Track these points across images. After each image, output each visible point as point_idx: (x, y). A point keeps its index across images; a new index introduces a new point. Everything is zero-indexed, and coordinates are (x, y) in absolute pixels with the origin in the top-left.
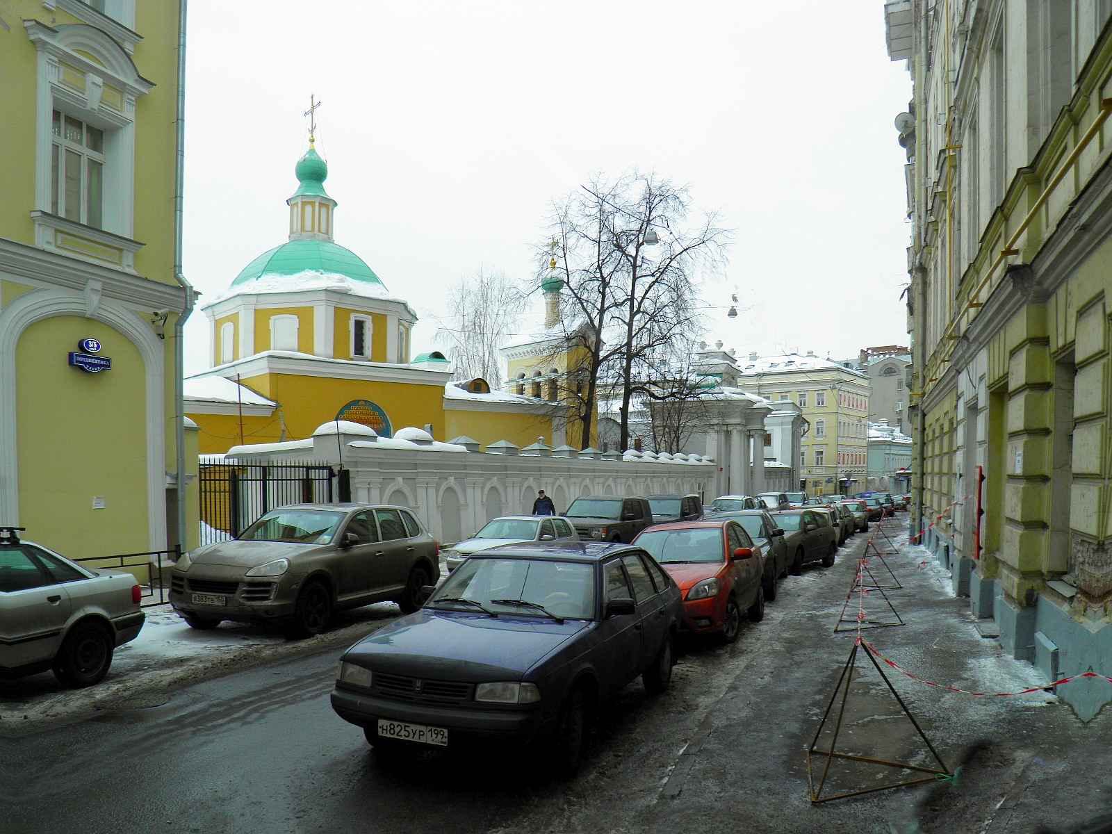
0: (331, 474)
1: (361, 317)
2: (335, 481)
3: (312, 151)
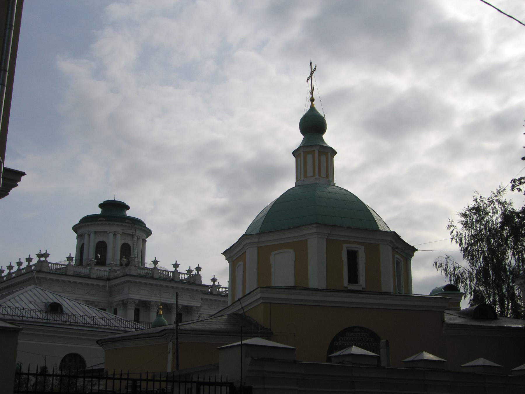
1: (353, 247)
3: (312, 108)
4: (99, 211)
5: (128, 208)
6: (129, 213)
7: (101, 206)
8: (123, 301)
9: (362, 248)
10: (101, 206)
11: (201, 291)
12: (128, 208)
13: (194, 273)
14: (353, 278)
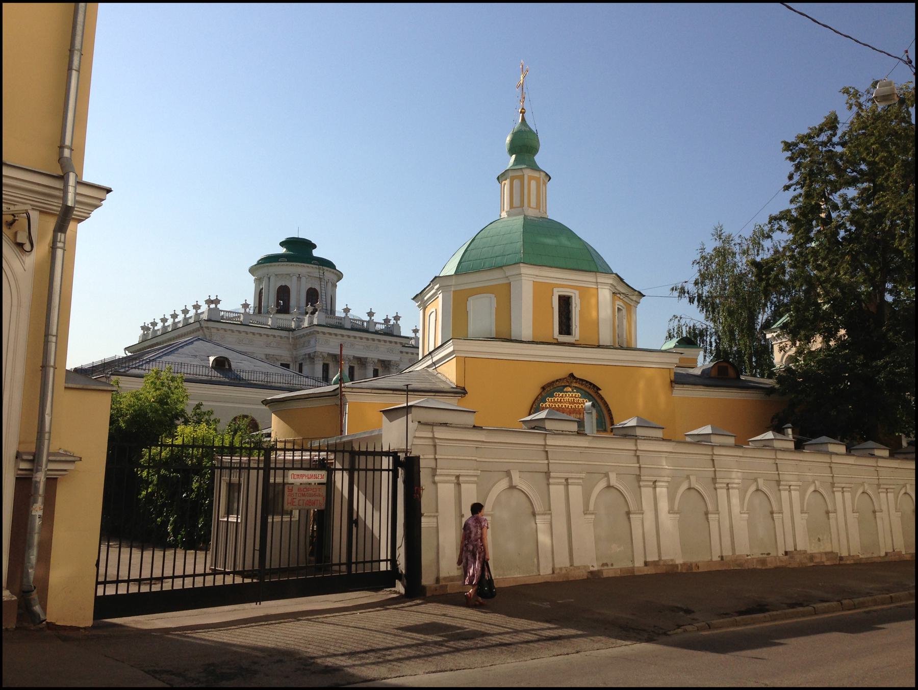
0: (397, 462)
2: (401, 472)
4: (283, 250)
5: (314, 246)
6: (316, 253)
7: (282, 244)
8: (309, 354)
9: (577, 292)
10: (282, 244)
11: (401, 343)
12: (314, 246)
13: (392, 323)
14: (565, 327)
